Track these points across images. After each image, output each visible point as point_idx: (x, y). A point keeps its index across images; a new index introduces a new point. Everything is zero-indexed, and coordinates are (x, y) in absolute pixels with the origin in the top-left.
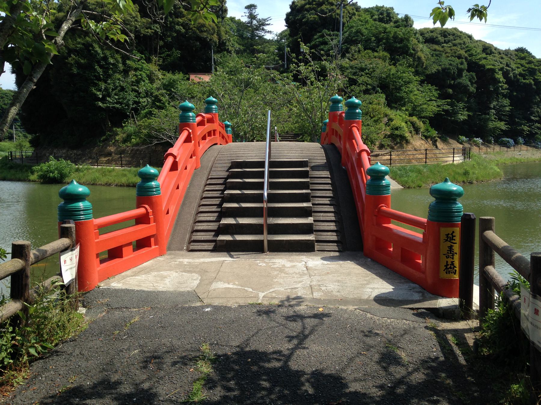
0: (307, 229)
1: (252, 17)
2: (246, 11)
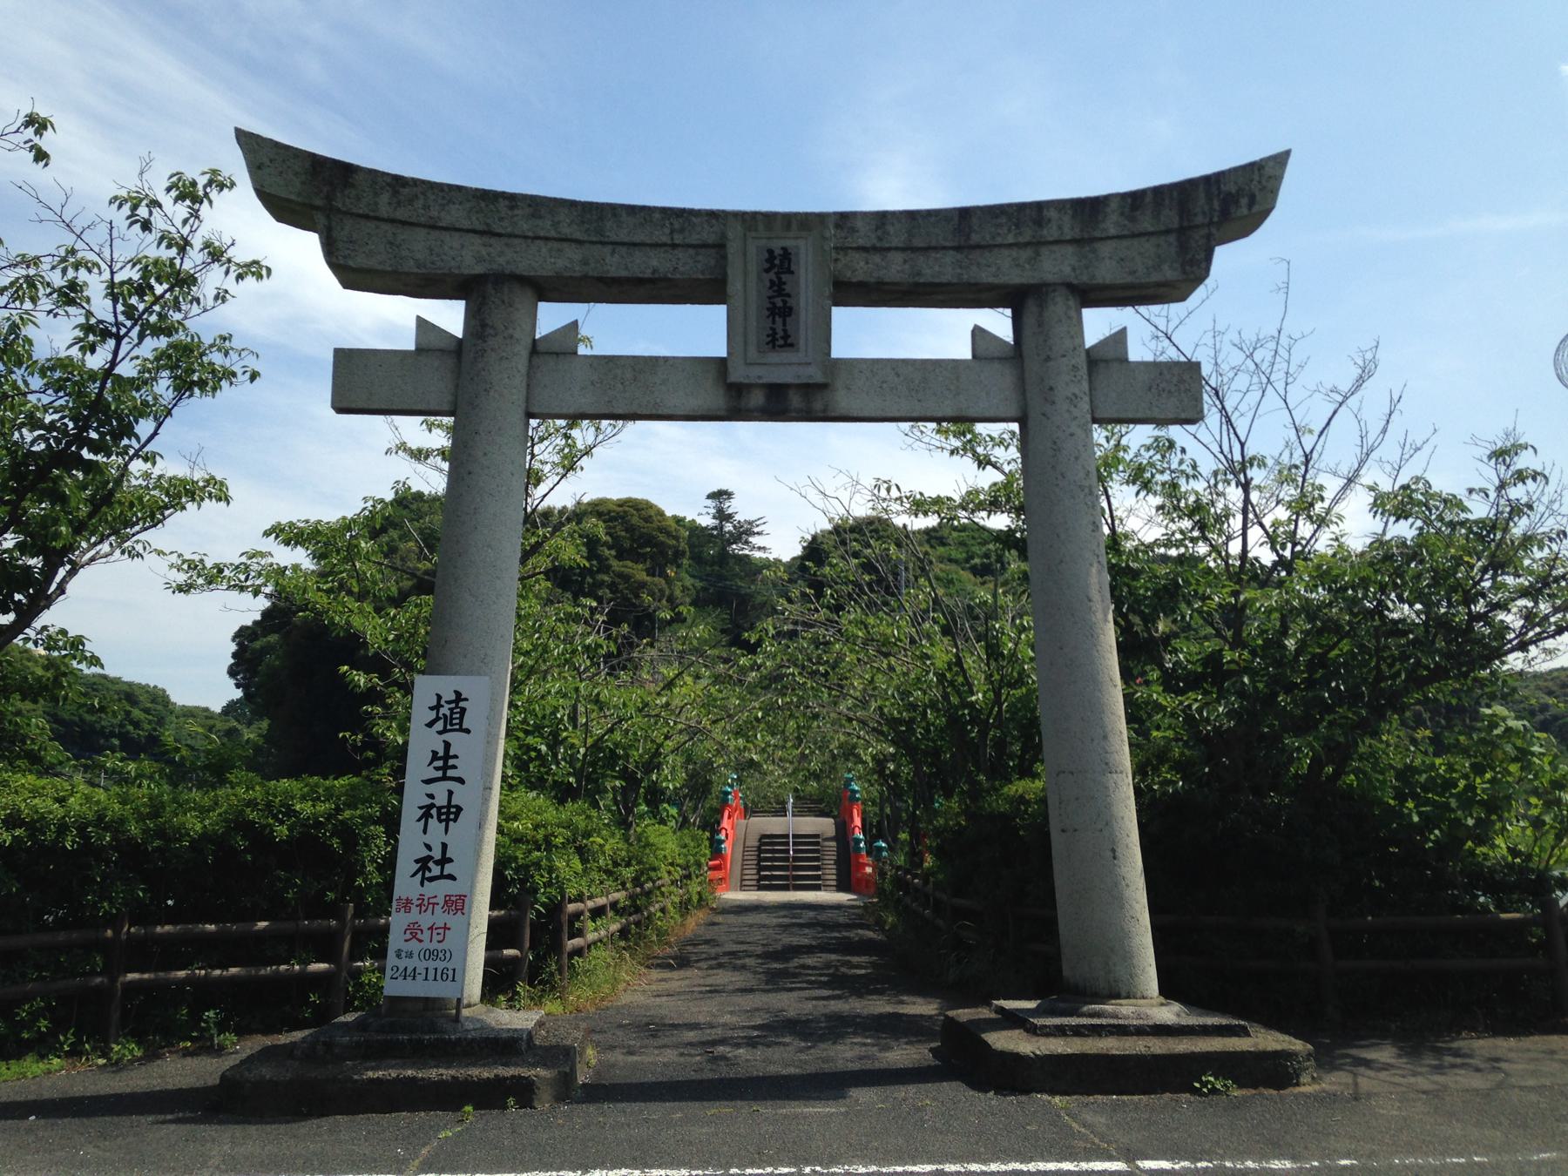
0: (818, 878)
1: (722, 516)
2: (709, 502)
